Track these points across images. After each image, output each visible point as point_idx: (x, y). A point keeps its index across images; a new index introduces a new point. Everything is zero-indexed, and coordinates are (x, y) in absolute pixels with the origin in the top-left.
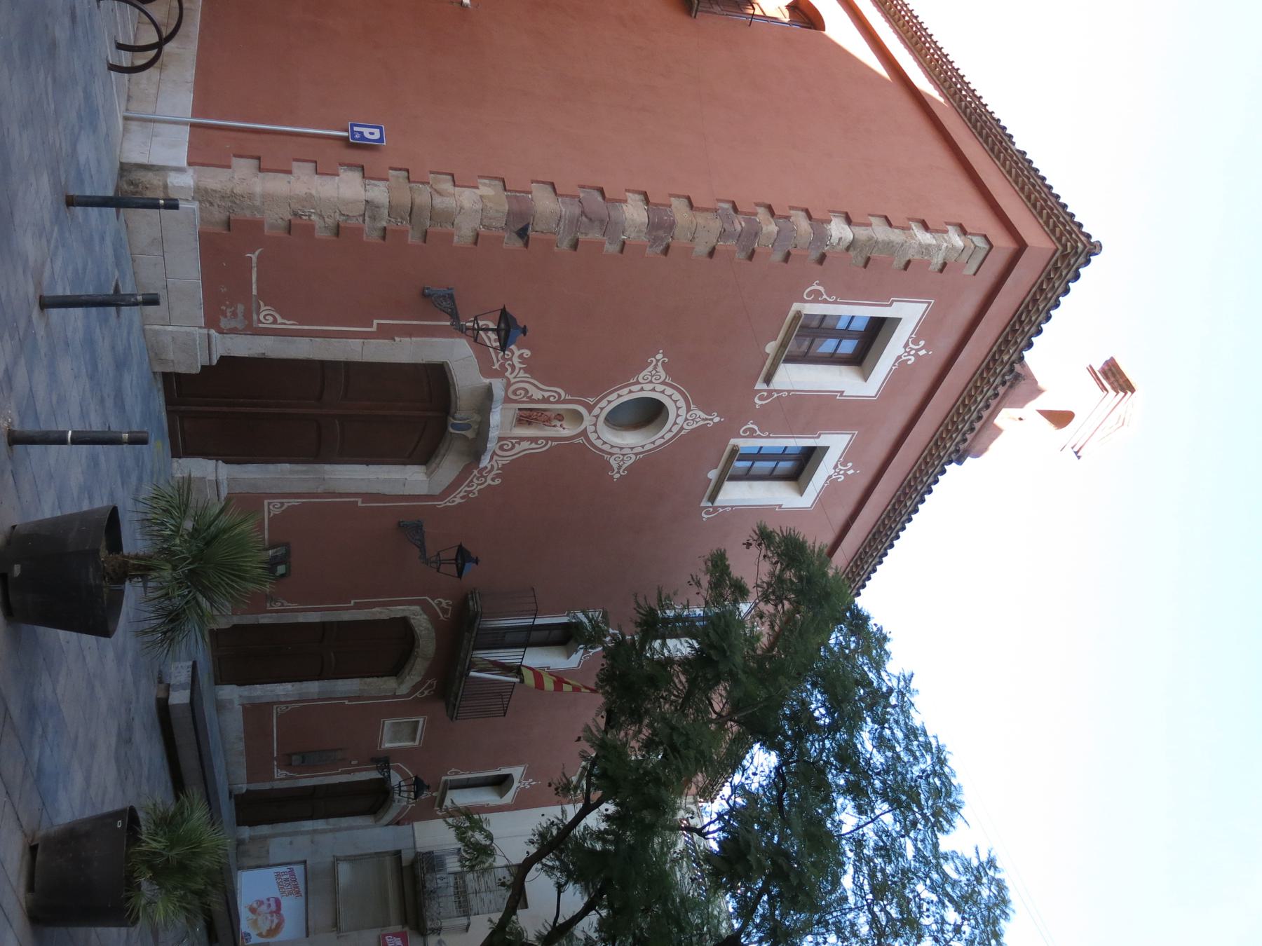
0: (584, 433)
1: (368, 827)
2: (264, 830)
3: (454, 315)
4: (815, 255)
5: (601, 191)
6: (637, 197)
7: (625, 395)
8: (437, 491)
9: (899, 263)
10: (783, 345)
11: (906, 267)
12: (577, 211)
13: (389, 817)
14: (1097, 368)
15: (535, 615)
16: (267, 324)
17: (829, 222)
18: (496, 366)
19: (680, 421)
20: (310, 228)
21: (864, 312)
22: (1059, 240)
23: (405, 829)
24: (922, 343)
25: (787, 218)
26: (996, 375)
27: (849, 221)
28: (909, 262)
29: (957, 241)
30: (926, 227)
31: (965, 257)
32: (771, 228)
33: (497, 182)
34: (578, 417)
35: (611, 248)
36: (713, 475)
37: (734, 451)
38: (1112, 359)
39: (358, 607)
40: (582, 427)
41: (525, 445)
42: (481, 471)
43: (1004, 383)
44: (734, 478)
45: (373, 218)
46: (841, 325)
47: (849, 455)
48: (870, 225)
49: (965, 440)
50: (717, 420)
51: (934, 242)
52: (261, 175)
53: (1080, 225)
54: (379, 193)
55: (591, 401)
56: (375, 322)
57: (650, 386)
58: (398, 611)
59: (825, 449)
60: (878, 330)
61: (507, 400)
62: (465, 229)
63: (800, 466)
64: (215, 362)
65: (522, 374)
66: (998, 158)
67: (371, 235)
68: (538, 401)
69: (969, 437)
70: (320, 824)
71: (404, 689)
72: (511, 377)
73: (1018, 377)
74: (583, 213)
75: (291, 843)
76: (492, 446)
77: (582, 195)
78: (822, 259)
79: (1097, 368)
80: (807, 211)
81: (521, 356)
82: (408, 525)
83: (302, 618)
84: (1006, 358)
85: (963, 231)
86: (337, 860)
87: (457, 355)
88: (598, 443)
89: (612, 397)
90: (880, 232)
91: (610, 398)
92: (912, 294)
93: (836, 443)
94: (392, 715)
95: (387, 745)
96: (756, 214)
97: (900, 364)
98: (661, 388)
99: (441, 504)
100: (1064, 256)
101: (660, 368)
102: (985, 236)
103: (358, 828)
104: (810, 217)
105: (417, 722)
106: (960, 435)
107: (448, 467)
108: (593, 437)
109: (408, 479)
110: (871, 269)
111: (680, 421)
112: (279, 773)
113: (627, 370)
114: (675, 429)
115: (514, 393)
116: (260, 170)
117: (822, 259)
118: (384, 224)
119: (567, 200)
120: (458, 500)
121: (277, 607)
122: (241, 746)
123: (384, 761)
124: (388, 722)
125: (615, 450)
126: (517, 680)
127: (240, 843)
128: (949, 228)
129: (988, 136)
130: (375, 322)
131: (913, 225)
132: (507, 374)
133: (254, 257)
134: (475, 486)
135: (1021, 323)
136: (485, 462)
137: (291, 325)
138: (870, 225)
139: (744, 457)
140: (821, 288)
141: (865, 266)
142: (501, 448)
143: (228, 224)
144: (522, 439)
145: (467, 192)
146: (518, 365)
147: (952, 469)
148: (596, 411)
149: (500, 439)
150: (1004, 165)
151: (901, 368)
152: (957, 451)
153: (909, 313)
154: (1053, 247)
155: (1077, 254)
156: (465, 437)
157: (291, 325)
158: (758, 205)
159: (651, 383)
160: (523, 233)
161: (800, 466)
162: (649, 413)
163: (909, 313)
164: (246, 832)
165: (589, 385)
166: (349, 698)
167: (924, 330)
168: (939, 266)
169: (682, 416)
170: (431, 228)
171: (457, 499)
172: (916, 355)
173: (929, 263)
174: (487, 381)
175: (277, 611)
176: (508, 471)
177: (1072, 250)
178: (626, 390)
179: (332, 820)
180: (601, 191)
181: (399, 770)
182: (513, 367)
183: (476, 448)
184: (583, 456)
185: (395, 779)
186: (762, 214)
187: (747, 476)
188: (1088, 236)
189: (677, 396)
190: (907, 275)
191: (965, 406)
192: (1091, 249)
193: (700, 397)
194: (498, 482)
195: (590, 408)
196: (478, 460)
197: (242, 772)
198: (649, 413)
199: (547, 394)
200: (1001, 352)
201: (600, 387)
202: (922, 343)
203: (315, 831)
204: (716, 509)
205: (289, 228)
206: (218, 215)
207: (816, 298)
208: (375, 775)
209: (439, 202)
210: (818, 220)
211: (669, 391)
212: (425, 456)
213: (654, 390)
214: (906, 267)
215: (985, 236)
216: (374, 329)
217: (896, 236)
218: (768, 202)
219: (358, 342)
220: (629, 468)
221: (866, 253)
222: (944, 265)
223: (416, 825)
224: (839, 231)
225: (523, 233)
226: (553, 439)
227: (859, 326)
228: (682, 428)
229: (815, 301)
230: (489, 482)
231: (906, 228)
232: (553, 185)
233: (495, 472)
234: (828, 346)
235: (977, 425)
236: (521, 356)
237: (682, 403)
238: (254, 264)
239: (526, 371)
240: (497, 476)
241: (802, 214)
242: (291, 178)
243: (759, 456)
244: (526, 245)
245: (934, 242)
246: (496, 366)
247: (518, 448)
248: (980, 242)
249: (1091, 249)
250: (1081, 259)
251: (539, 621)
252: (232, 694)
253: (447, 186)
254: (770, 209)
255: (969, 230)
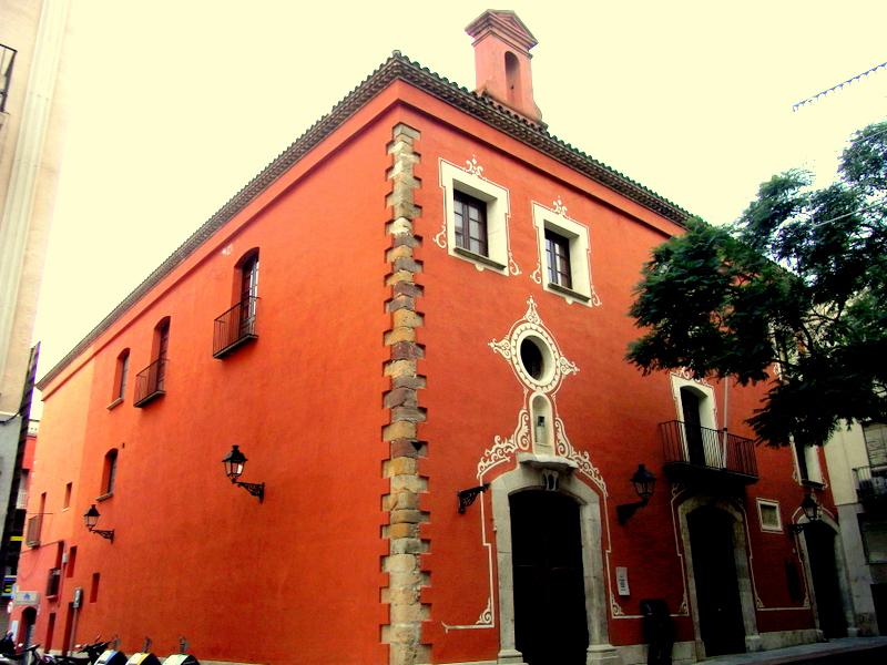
0: (548, 394)
1: (841, 541)
2: (849, 615)
3: (478, 490)
4: (416, 244)
5: (385, 394)
6: (387, 368)
7: (520, 367)
8: (596, 497)
9: (416, 185)
10: (477, 258)
11: (419, 180)
12: (400, 409)
13: (830, 521)
14: (473, 40)
15: (676, 422)
16: (492, 618)
17: (393, 235)
18: (508, 459)
19: (534, 327)
20: (424, 591)
21: (451, 206)
22: (392, 78)
23: (839, 510)
24: (468, 162)
25: (393, 264)
26: (486, 110)
27: (391, 222)
28: (416, 178)
29: (397, 148)
30: (389, 170)
31: (409, 140)
32: (402, 276)
33: (385, 467)
34: (539, 402)
35: (422, 385)
36: (570, 300)
37: (552, 286)
38: (466, 30)
39: (682, 551)
40: (545, 396)
41: (560, 436)
42: (581, 467)
43: (491, 103)
44: (569, 284)
45: (417, 548)
46: (460, 219)
47: (548, 205)
48: (393, 207)
49: (532, 125)
50: (532, 301)
51: (401, 162)
52: (393, 624)
53: (382, 66)
54: (399, 544)
55: (526, 391)
56: (485, 544)
57: (513, 350)
58: (683, 521)
59: (546, 222)
60: (464, 196)
61: (530, 450)
62: (416, 485)
63: (560, 240)
64: (520, 653)
65: (511, 441)
66: (337, 124)
67: (425, 550)
68: (529, 428)
69: (529, 123)
70: (842, 575)
71: (738, 516)
72: (515, 448)
73: (485, 94)
74: (402, 405)
75: (857, 596)
76: (562, 459)
77: (389, 407)
78: (419, 238)
79: (473, 40)
80: (387, 251)
81: (500, 443)
82: (621, 516)
83: (693, 592)
84: (474, 104)
85: (392, 143)
86: (868, 562)
87: (506, 484)
88: (555, 384)
89: (522, 375)
90: (396, 200)
91: (518, 370)
92: (436, 173)
93: (541, 215)
94: (758, 527)
95: (780, 528)
96: (392, 286)
97: (483, 175)
98: (513, 342)
99: (605, 494)
100: (404, 74)
101: (500, 344)
102: (394, 128)
103: (842, 544)
104: (391, 249)
105: (762, 506)
106: (531, 134)
107: (581, 490)
108: (551, 388)
109: (591, 518)
110: (421, 207)
111: (534, 327)
112: (806, 605)
113: (500, 366)
114: (541, 330)
115: (525, 445)
116: (388, 587)
117: (419, 238)
118: (419, 541)
119: (394, 416)
120: (602, 481)
121: (686, 608)
122: (789, 633)
123: (791, 529)
124: (764, 527)
125: (559, 372)
126: (725, 433)
127: (860, 634)
128: (390, 152)
129: (323, 132)
130: (485, 544)
131: (390, 177)
132: (513, 451)
133: (447, 627)
134: (591, 471)
135: (450, 96)
136: (573, 464)
137: (491, 602)
138: (393, 207)
139: (554, 278)
140: (438, 236)
141: (420, 208)
142: (563, 453)
143: (428, 646)
144: (556, 437)
145: (393, 485)
146: (506, 444)
147: (552, 131)
148: (533, 387)
149: (557, 454)
150: (343, 120)
151: (571, 214)
152: (540, 129)
153: (449, 175)
154: (398, 82)
155: (402, 65)
156: (557, 480)
157: (491, 602)
158: (385, 284)
159: (511, 350)
160: (418, 446)
161: (560, 240)
162: (533, 355)
163: (449, 175)
164: (852, 630)
165: (516, 393)
166: (748, 555)
167: (459, 162)
168: (417, 157)
169: (531, 326)
170: (422, 508)
171: (601, 483)
172: (476, 166)
173: (414, 164)
174: (518, 466)
175: (690, 609)
176: (579, 448)
177: (401, 70)
178: (517, 366)
179: (838, 566)
180: (385, 394)
181: (796, 518)
182: (508, 447)
183: (567, 472)
184: (565, 398)
185: (803, 519)
186: (392, 281)
187: (568, 275)
188: (389, 59)
189: (518, 331)
190: (423, 178)
191: (508, 128)
192: (398, 56)
193: (518, 313)
194: (587, 454)
195: (531, 391)
196: (573, 468)
197: (808, 632)
198: (533, 355)
199: (524, 423)
200: (470, 108)
201: (517, 386)
202: (468, 162)
203: (848, 578)
204: (593, 296)
205: (427, 605)
206: (421, 651)
207: (444, 239)
208: (802, 536)
209: (403, 503)
210: (393, 243)
211: (515, 336)
212: (573, 507)
213: (515, 347)
214: (419, 180)
215: (394, 128)
216: (489, 545)
217: (399, 188)
218: (381, 395)
219: (500, 557)
220: (570, 360)
221: (412, 208)
222: (415, 153)
223: (837, 503)
224: (399, 228)
225: (418, 446)
226: (554, 416)
227: (459, 206)
228: (540, 325)
229: (446, 239)
230: (587, 460)
231: (393, 182)
232: (383, 462)
233: (580, 456)
234: (474, 230)
235: (521, 118)
236: (500, 443)
237: (522, 327)
238: (453, 627)
239: (509, 438)
240: (582, 454)
241: (389, 254)
242: (393, 605)
243: (553, 268)
244: (426, 443)
245: (401, 162)
246: (508, 459)
247: (563, 441)
248: (398, 131)
249: (398, 56)
250: (405, 62)
251: (682, 419)
252: (753, 638)
253: (390, 501)
254: (388, 277)
255: (389, 297)
